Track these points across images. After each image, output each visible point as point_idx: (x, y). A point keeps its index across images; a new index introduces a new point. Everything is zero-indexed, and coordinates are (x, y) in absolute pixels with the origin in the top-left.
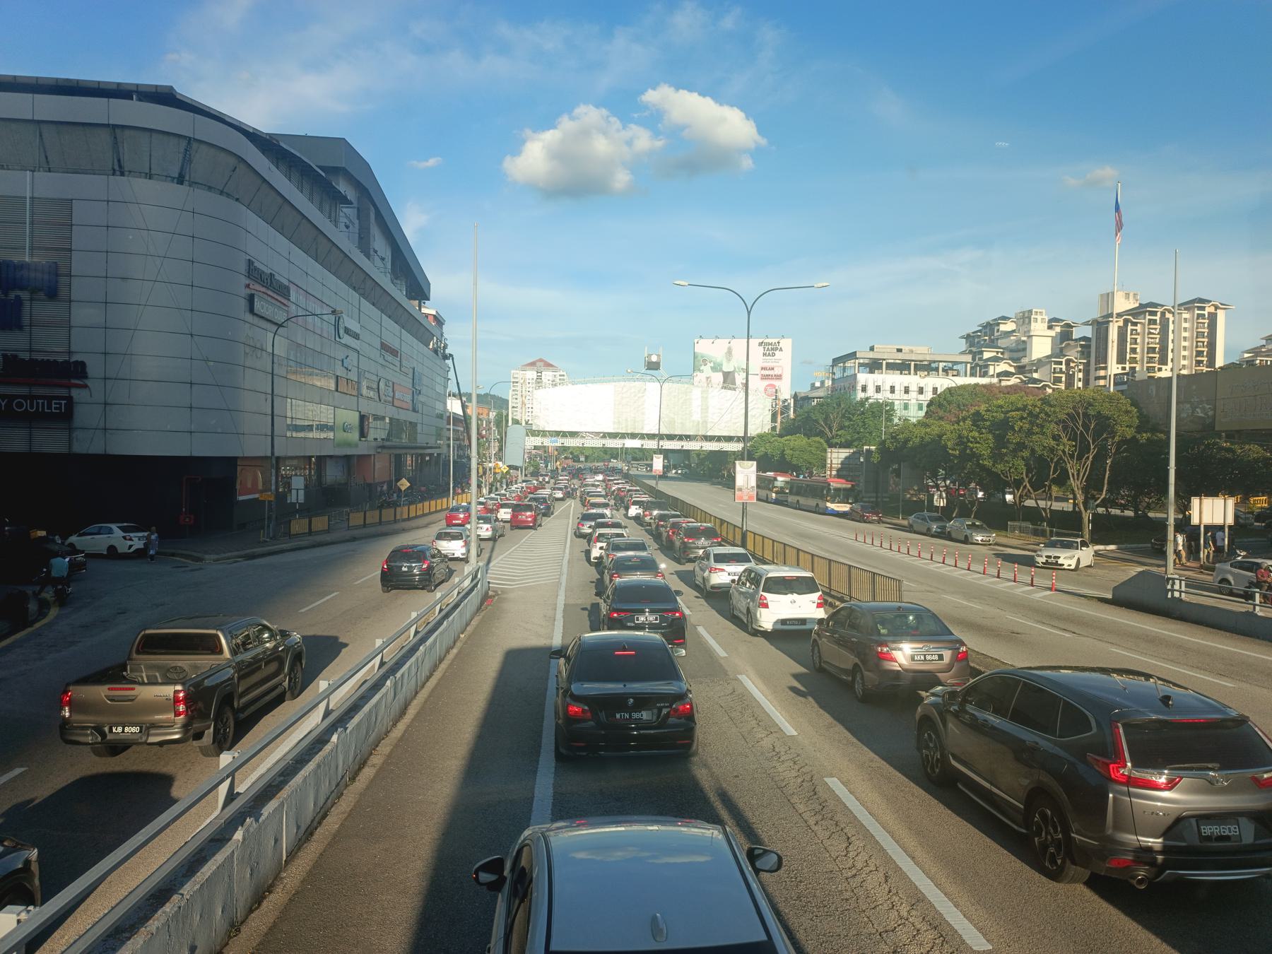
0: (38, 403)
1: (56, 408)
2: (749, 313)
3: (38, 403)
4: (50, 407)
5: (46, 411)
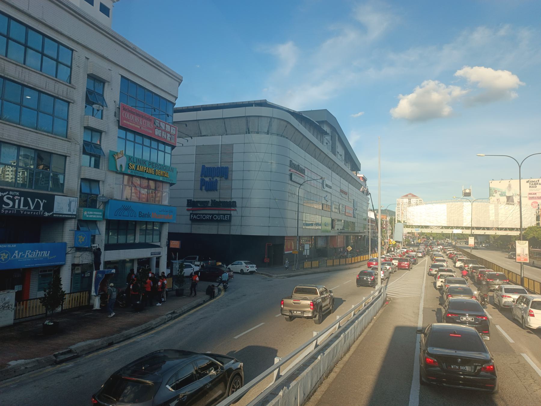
0: (14, 193)
1: (226, 218)
2: (520, 167)
3: (14, 193)
4: (224, 218)
5: (223, 219)
